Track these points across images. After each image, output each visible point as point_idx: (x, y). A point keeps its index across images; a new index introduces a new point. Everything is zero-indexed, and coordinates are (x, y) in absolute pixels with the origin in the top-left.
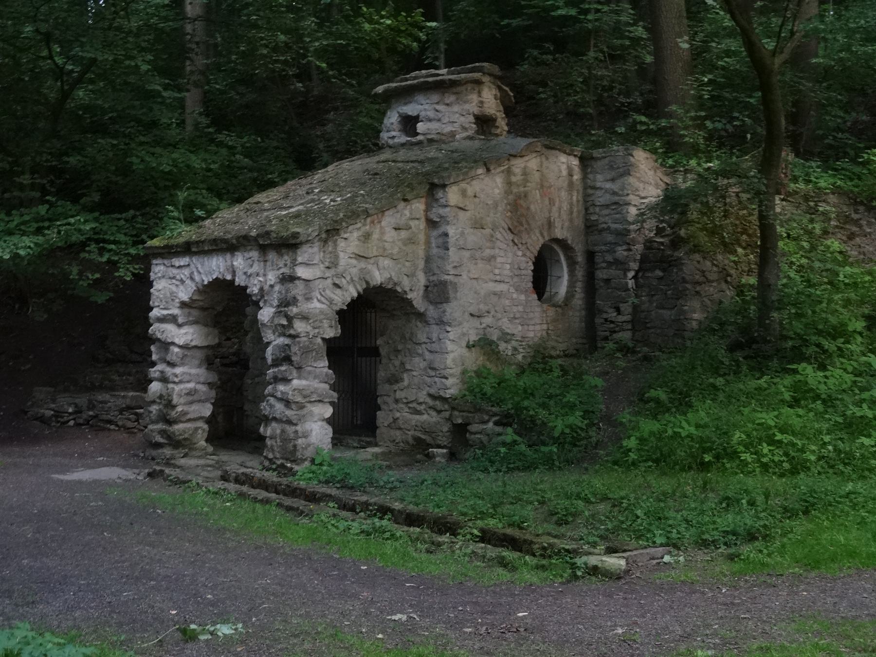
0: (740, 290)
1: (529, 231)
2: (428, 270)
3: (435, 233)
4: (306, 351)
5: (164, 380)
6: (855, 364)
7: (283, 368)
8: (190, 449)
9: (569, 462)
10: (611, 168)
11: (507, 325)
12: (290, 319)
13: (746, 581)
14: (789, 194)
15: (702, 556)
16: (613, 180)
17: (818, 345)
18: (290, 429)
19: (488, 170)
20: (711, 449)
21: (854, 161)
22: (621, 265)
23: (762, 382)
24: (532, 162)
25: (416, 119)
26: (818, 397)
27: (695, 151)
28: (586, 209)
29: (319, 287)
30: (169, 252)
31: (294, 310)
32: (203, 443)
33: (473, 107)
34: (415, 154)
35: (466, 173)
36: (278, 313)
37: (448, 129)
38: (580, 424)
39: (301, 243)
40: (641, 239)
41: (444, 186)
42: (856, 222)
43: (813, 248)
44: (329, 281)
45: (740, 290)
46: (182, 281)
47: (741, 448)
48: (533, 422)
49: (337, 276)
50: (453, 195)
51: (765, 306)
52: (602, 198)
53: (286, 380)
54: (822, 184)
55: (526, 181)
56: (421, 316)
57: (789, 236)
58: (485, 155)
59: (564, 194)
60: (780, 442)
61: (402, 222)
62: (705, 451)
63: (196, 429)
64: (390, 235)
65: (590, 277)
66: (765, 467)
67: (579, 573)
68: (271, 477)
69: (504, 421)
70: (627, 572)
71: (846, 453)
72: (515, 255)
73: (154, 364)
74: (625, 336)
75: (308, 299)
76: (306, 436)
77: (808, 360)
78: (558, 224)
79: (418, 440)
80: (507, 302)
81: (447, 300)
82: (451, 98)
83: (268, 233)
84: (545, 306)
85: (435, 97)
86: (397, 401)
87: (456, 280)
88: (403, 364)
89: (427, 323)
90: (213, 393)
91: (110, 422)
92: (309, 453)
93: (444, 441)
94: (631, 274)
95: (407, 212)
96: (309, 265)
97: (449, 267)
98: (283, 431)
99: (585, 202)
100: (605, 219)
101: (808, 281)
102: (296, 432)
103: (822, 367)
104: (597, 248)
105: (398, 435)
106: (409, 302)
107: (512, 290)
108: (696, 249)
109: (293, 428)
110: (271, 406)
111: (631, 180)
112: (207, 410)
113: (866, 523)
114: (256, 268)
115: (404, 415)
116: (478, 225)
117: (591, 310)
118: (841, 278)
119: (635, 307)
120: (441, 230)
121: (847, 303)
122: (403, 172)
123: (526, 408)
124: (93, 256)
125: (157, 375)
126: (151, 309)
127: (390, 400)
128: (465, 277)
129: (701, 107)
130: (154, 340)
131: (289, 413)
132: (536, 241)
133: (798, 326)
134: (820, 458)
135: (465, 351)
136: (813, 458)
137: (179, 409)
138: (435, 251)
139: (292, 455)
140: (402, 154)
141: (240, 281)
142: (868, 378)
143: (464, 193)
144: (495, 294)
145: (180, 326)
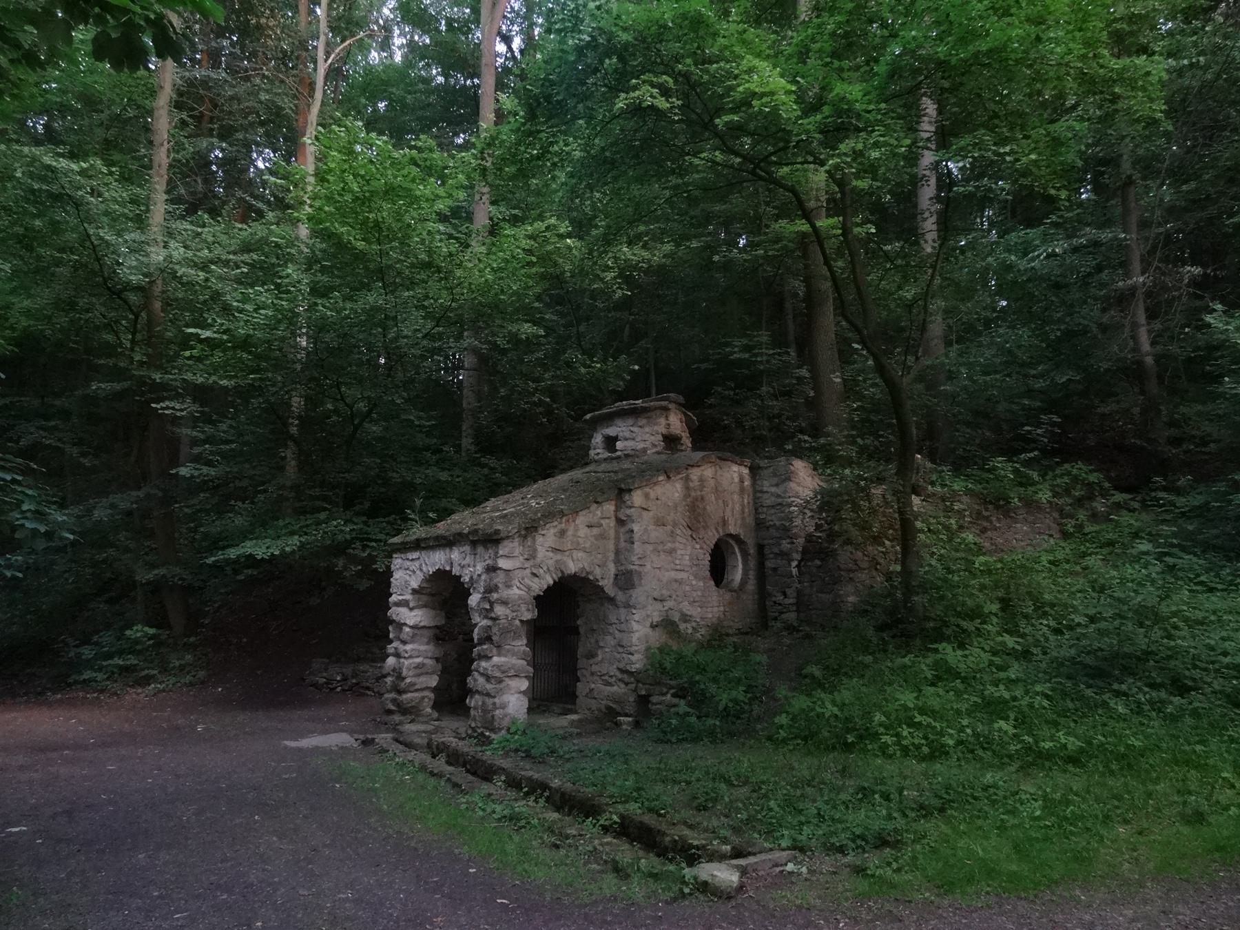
0: (889, 576)
1: (706, 527)
2: (617, 561)
3: (622, 530)
4: (505, 632)
5: (397, 655)
6: (992, 643)
7: (485, 647)
8: (417, 716)
9: (731, 735)
10: (775, 475)
11: (686, 608)
12: (491, 604)
13: (870, 908)
14: (929, 496)
15: (827, 863)
16: (777, 485)
17: (958, 626)
18: (489, 701)
19: (669, 477)
20: (854, 729)
21: (982, 469)
22: (785, 555)
23: (906, 660)
24: (708, 471)
25: (616, 439)
26: (957, 675)
27: (850, 463)
28: (756, 509)
29: (515, 577)
30: (405, 548)
31: (495, 596)
32: (429, 710)
33: (661, 429)
34: (615, 466)
35: (648, 480)
36: (484, 598)
37: (640, 446)
38: (742, 698)
39: (502, 539)
40: (802, 534)
41: (630, 490)
42: (987, 518)
43: (950, 540)
44: (528, 571)
45: (889, 576)
46: (414, 572)
47: (882, 730)
48: (704, 695)
49: (534, 566)
50: (637, 498)
51: (909, 590)
52: (768, 500)
53: (488, 658)
54: (956, 487)
55: (702, 487)
56: (612, 600)
57: (929, 530)
58: (668, 465)
59: (736, 497)
60: (920, 723)
61: (595, 520)
62: (849, 731)
63: (423, 698)
64: (583, 531)
65: (761, 565)
66: (905, 751)
67: (687, 891)
68: (465, 747)
69: (681, 693)
70: (741, 888)
71: (985, 737)
72: (694, 548)
73: (391, 642)
74: (791, 616)
75: (509, 586)
76: (503, 707)
77: (947, 639)
78: (731, 522)
79: (609, 708)
80: (687, 588)
81: (633, 586)
82: (642, 422)
83: (476, 531)
84: (722, 591)
85: (630, 421)
86: (592, 674)
87: (640, 569)
88: (597, 641)
89: (617, 606)
90: (440, 666)
91: (368, 688)
92: (506, 722)
93: (630, 709)
94: (794, 564)
95: (599, 513)
96: (510, 558)
97: (634, 559)
98: (484, 703)
99: (755, 503)
100: (773, 518)
101: (948, 569)
102: (494, 704)
103: (962, 646)
104: (766, 542)
105: (594, 705)
106: (601, 589)
107: (691, 578)
108: (849, 542)
109: (491, 700)
110: (475, 680)
111: (792, 485)
112: (433, 681)
113: (1006, 829)
114: (468, 560)
115: (598, 686)
116: (660, 522)
117: (762, 594)
118: (977, 565)
119: (799, 593)
120: (627, 528)
121: (983, 587)
122: (598, 479)
123: (698, 682)
124: (356, 552)
125: (392, 651)
126: (391, 595)
127: (587, 674)
128: (648, 566)
129: (853, 428)
130: (392, 622)
131: (489, 686)
132: (712, 537)
133: (938, 610)
134: (960, 742)
135: (649, 630)
136: (951, 742)
137: (408, 680)
138: (623, 544)
139: (491, 725)
140: (603, 467)
141: (456, 571)
142: (1005, 657)
143: (647, 496)
144: (676, 581)
145: (411, 609)
